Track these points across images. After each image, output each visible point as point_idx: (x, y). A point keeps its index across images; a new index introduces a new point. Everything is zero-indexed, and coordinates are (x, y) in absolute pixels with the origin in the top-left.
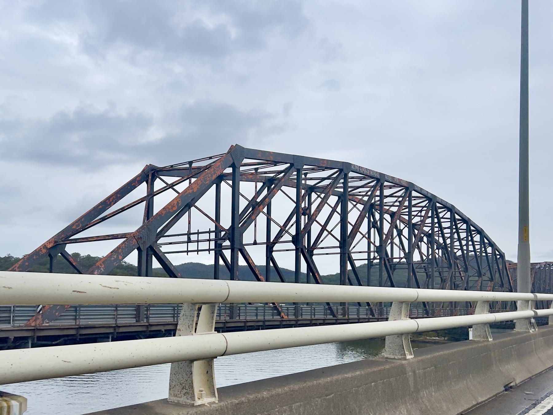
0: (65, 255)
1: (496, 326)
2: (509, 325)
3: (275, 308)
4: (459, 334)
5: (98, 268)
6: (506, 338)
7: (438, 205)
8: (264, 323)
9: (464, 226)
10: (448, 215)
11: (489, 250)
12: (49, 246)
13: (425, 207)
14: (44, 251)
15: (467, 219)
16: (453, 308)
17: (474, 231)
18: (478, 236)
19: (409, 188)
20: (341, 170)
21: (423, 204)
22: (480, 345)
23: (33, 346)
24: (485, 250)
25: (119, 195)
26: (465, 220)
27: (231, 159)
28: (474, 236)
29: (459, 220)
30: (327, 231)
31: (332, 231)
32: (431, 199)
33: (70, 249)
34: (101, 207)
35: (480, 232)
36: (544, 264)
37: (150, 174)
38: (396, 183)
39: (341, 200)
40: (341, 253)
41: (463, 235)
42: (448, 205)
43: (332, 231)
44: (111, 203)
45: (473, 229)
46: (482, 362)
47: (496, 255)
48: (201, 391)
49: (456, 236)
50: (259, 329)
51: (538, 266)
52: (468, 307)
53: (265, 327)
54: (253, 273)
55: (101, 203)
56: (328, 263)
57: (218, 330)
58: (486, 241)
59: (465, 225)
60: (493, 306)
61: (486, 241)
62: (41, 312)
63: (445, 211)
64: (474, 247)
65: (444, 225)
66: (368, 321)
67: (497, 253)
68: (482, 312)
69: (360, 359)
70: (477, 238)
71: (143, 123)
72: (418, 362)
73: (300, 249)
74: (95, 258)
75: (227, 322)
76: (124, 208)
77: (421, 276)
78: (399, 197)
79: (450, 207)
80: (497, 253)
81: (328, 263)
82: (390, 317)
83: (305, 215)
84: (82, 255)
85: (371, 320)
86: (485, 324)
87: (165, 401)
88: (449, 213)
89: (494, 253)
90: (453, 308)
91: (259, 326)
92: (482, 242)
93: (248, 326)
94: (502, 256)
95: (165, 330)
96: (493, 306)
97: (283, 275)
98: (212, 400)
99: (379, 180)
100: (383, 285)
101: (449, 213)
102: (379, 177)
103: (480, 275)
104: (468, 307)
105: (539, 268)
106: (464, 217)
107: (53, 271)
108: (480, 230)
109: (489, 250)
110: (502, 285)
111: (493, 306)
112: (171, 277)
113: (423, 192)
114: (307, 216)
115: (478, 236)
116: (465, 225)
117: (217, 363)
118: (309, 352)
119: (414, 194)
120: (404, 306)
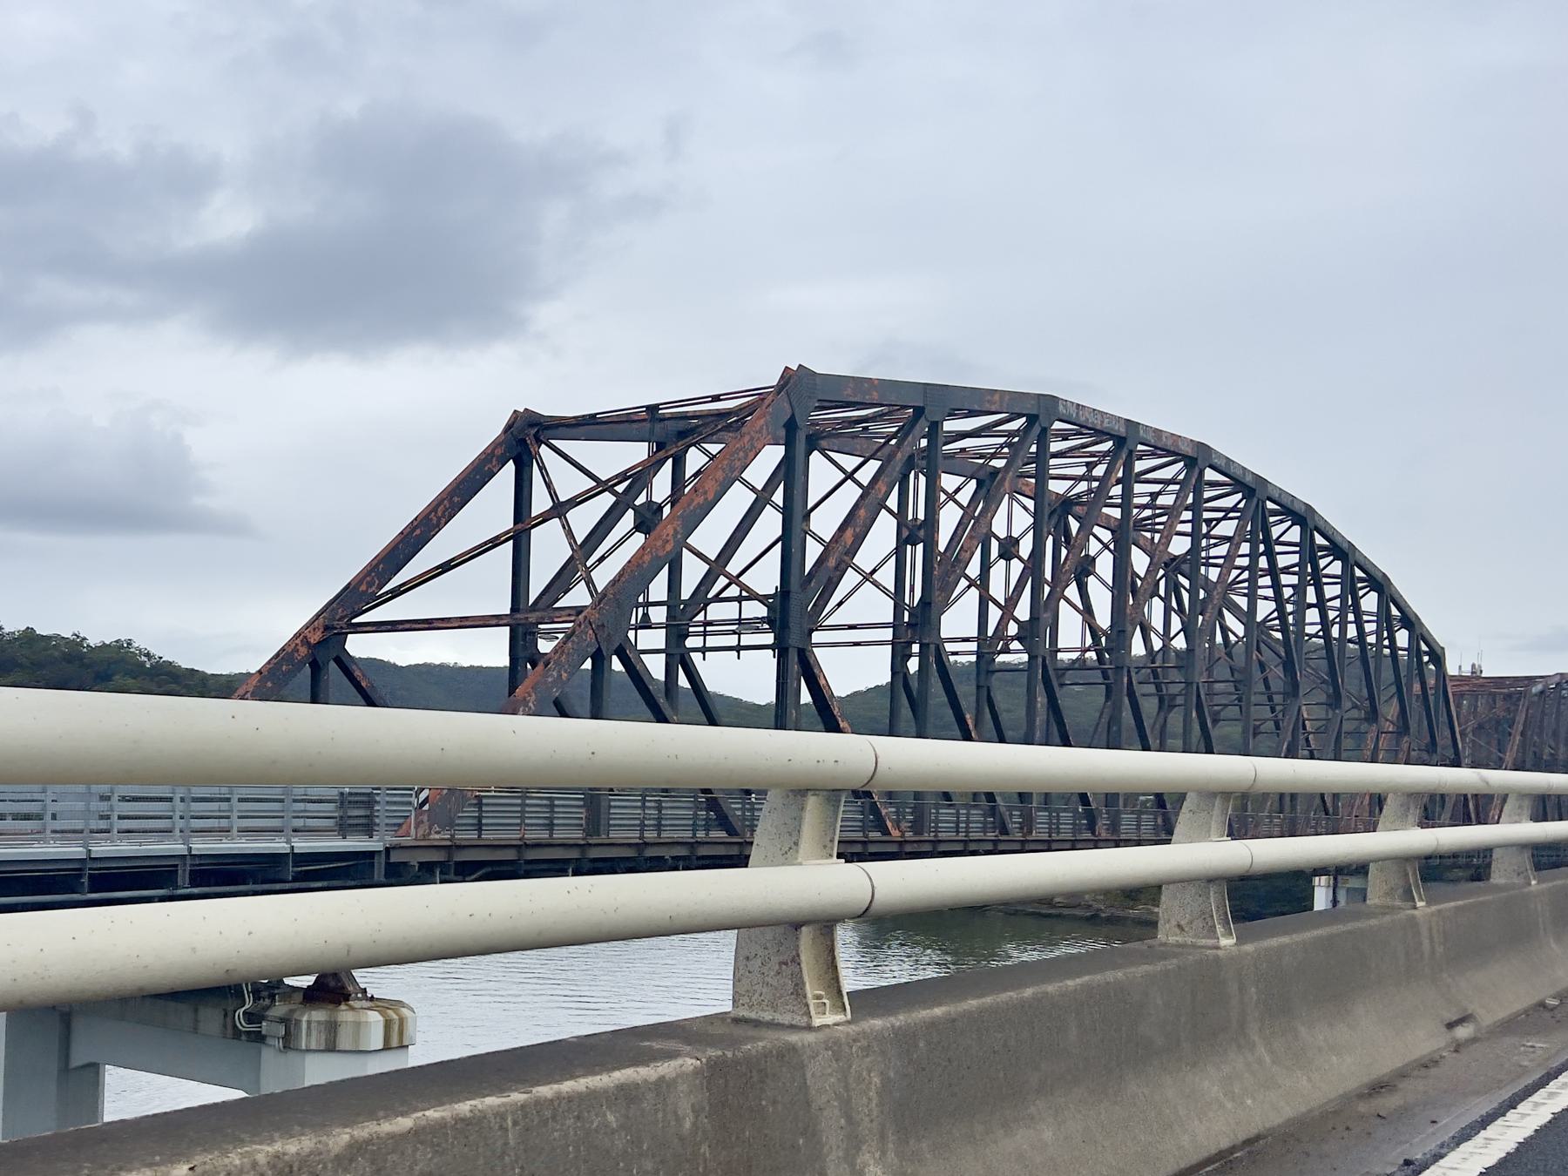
0: (345, 664)
1: (1435, 870)
2: (1472, 866)
3: (713, 804)
4: (1124, 913)
5: (525, 702)
6: (1281, 939)
7: (1270, 505)
8: (583, 852)
9: (1336, 568)
10: (1294, 534)
11: (1402, 638)
12: (315, 638)
13: (1234, 509)
14: (303, 651)
15: (1345, 546)
16: (1094, 817)
17: (1361, 580)
18: (1374, 596)
19: (1196, 458)
20: (1032, 419)
21: (1229, 502)
22: (1373, 922)
23: (575, 874)
24: (1392, 638)
25: (456, 499)
26: (1341, 550)
27: (786, 405)
28: (1361, 593)
29: (1322, 548)
30: (858, 570)
31: (874, 571)
32: (1251, 488)
33: (358, 646)
34: (418, 532)
35: (1379, 583)
36: (1557, 679)
37: (524, 439)
38: (1166, 448)
39: (984, 491)
40: (893, 643)
41: (1331, 591)
42: (1296, 507)
43: (874, 571)
44: (439, 519)
45: (1363, 576)
46: (1205, 1019)
47: (1419, 653)
48: (818, 997)
49: (1311, 596)
50: (676, 869)
51: (1539, 687)
52: (1158, 814)
53: (695, 863)
54: (656, 704)
55: (412, 526)
56: (855, 668)
57: (849, 857)
58: (1395, 612)
59: (1338, 564)
60: (1433, 808)
61: (1395, 612)
62: (426, 807)
63: (1282, 521)
64: (1360, 629)
65: (1282, 561)
66: (1074, 845)
67: (1424, 648)
68: (1203, 835)
69: (931, 973)
70: (1370, 602)
71: (188, 180)
72: (1432, 914)
73: (932, 647)
74: (49, 638)
75: (646, 844)
76: (498, 537)
77: (1083, 702)
78: (1011, 434)
79: (1302, 510)
80: (1424, 648)
81: (855, 668)
82: (755, 854)
83: (914, 544)
84: (7, 630)
85: (1054, 846)
86: (1211, 880)
87: (721, 1017)
88: (1297, 529)
89: (1413, 649)
90: (1094, 817)
91: (567, 861)
92: (1383, 617)
93: (699, 858)
94: (1437, 657)
95: (421, 864)
96: (1248, 813)
97: (718, 709)
98: (840, 1018)
99: (1125, 441)
100: (1528, 766)
101: (1297, 529)
102: (1122, 431)
103: (1373, 715)
104: (1158, 814)
105: (1542, 692)
106: (1338, 540)
107: (1344, 755)
108: (1379, 578)
109: (1402, 638)
110: (1432, 747)
111: (1248, 813)
112: (828, 730)
113: (1232, 471)
114: (920, 547)
115: (1374, 596)
116: (1338, 564)
117: (78, 1025)
118: (642, 967)
119: (1210, 475)
120: (1218, 802)
